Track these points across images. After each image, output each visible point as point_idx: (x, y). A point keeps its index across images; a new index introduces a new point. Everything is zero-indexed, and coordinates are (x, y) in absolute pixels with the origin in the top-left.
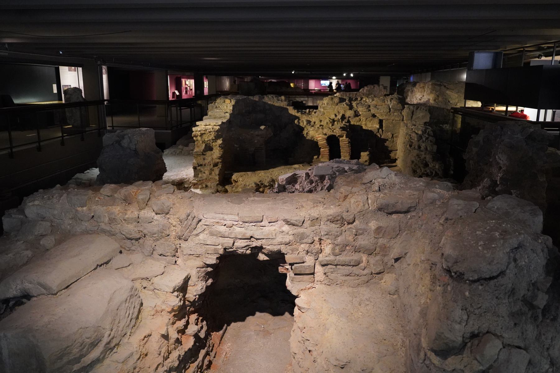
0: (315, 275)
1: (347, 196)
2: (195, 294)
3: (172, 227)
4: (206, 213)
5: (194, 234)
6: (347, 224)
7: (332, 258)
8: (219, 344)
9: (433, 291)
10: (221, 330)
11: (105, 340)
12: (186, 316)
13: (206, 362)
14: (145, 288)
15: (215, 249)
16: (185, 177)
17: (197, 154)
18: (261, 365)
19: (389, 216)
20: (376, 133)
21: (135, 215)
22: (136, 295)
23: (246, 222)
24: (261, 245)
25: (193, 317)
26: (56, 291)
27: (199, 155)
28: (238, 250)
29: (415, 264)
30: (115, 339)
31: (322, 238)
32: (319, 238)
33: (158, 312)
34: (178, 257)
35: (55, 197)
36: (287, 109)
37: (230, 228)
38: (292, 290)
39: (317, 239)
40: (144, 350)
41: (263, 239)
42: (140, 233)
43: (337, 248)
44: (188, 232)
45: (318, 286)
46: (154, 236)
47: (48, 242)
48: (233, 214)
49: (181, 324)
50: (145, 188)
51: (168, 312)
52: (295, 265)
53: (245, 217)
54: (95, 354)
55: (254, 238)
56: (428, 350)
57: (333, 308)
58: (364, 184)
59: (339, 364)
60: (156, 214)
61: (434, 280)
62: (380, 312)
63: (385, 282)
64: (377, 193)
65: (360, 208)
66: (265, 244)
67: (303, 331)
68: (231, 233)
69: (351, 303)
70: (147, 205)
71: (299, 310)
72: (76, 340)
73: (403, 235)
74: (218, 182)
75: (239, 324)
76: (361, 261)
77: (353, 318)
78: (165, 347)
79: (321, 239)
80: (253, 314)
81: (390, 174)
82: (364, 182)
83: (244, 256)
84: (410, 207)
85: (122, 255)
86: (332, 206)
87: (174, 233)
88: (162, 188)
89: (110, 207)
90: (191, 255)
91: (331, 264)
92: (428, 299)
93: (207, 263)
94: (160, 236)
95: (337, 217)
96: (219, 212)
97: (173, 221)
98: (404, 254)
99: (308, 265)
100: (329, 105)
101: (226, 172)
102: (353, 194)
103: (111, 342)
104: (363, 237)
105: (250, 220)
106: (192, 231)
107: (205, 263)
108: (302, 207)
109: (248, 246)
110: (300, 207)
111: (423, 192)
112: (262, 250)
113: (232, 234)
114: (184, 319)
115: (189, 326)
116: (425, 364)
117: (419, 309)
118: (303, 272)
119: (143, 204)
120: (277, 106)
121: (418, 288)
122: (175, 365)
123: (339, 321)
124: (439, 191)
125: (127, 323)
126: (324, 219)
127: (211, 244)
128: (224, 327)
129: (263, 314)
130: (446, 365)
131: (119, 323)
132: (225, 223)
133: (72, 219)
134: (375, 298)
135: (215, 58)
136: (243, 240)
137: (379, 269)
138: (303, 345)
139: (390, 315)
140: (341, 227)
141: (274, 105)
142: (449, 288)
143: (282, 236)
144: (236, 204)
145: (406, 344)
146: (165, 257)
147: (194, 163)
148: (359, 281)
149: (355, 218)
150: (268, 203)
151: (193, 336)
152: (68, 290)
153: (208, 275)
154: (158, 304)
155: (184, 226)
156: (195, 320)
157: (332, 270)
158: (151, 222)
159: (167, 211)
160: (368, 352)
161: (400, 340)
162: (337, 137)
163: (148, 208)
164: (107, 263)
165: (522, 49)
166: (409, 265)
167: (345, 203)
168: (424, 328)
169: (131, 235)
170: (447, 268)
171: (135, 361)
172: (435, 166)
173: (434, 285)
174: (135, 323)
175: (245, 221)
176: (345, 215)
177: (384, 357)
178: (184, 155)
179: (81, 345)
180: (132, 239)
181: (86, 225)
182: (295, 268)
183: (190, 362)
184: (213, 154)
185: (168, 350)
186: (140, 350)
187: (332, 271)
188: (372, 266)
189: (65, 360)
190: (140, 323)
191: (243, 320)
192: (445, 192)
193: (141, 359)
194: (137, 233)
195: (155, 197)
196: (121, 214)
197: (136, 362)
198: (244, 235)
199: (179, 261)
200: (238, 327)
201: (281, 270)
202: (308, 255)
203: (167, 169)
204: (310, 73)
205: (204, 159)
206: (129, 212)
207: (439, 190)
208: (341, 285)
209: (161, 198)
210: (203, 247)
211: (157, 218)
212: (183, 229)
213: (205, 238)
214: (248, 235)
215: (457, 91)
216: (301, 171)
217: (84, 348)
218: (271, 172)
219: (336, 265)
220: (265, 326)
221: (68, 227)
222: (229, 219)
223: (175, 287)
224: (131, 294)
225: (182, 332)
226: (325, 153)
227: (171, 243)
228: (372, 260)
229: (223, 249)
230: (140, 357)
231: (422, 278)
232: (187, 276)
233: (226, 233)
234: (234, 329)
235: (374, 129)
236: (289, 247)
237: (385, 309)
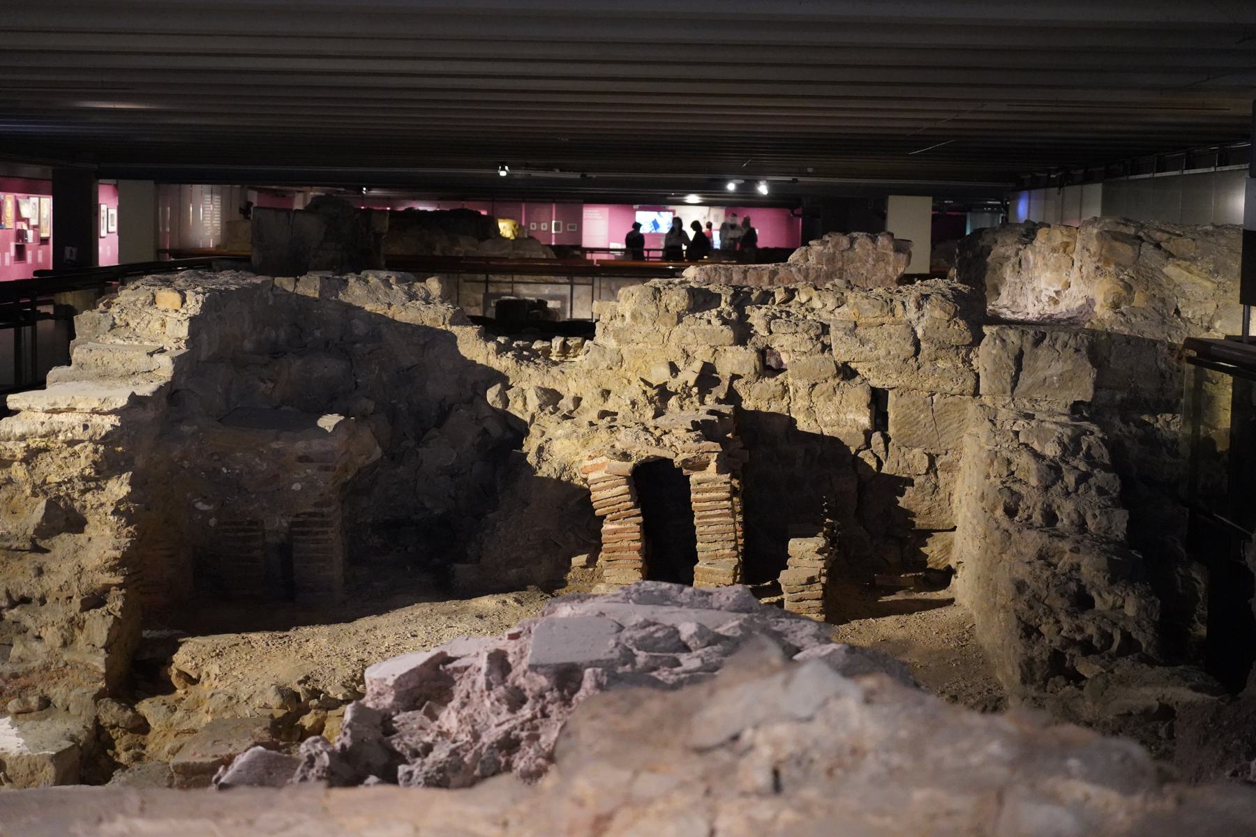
17: (9, 549)
20: (858, 451)
27: (17, 550)
36: (453, 338)
74: (102, 684)
101: (145, 633)
120: (407, 324)
141: (393, 321)
162: (680, 470)
172: (1122, 607)
204: (578, 176)
205: (40, 572)
207: (1078, 789)
218: (362, 632)
226: (625, 544)
235: (848, 433)
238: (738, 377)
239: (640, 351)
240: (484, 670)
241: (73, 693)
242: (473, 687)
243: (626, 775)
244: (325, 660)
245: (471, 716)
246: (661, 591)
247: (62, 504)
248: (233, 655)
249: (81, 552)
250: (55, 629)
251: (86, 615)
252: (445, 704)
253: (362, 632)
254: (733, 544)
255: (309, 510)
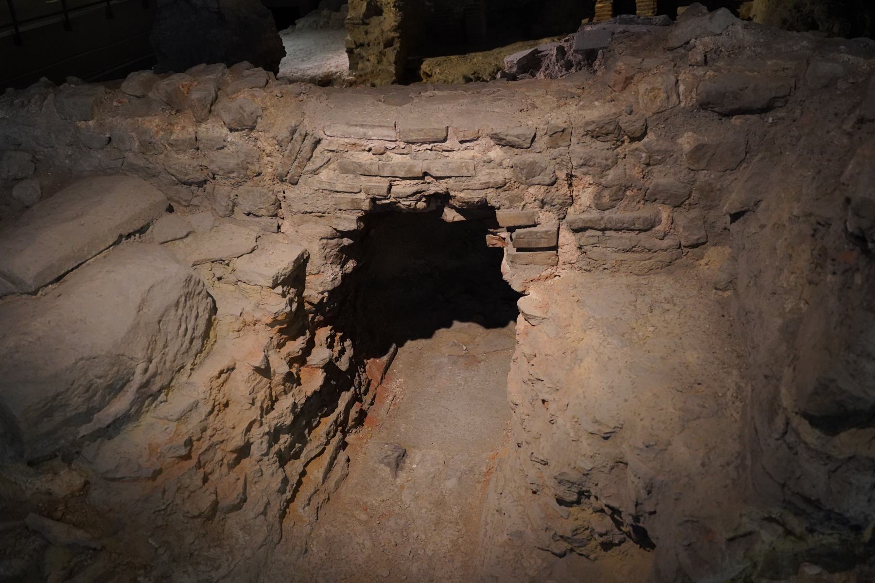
0: (559, 250)
1: (632, 78)
2: (321, 289)
3: (265, 158)
4: (329, 126)
5: (308, 171)
6: (628, 140)
7: (595, 214)
8: (382, 379)
9: (817, 284)
10: (384, 355)
11: (138, 379)
12: (307, 331)
13: (353, 414)
14: (219, 279)
15: (353, 201)
16: (333, 70)
17: (354, 24)
18: (459, 420)
19: (724, 119)
21: (190, 134)
22: (199, 294)
23: (413, 143)
24: (445, 190)
25: (323, 333)
26: (33, 287)
27: (357, 24)
28: (399, 202)
29: (776, 226)
30: (158, 378)
31: (573, 173)
32: (567, 174)
33: (246, 325)
34: (283, 219)
35: (33, 100)
37: (381, 157)
38: (512, 281)
39: (562, 175)
40: (220, 396)
41: (450, 177)
42: (205, 171)
43: (606, 193)
44: (297, 166)
45: (564, 273)
46: (232, 175)
47: (26, 191)
48: (383, 126)
49: (296, 346)
50: (208, 77)
51: (267, 324)
52: (517, 230)
53: (410, 131)
54: (120, 405)
55: (432, 176)
56: (794, 414)
57: (593, 317)
58: (671, 49)
59: (599, 430)
60: (231, 130)
61: (821, 259)
62: (694, 326)
63: (707, 264)
64: (700, 69)
65: (659, 104)
66: (454, 188)
67: (532, 362)
68: (384, 166)
69: (632, 308)
70: (210, 111)
71: (526, 320)
72: (74, 381)
73: (754, 161)
74: (394, 78)
75: (422, 342)
76: (657, 219)
77: (635, 337)
78: (264, 389)
79: (572, 176)
80: (448, 325)
81: (732, 24)
82: (671, 45)
83: (413, 213)
84: (774, 98)
85: (172, 216)
86: (596, 103)
87: (270, 170)
88: (243, 76)
89: (140, 119)
90: (306, 212)
91: (592, 228)
92: (803, 302)
93: (341, 228)
94: (242, 175)
95: (607, 126)
96: (355, 123)
97: (265, 144)
98: (752, 204)
99: (544, 229)
101: (409, 58)
102: (645, 74)
103: (151, 384)
104: (664, 169)
105: (422, 137)
106: (304, 163)
107: (335, 229)
108: (534, 107)
109: (420, 192)
110: (530, 107)
111: (807, 61)
112: (450, 201)
113: (386, 169)
114: (302, 338)
115: (314, 351)
116: (785, 441)
117: (779, 321)
118: (533, 246)
119: (203, 110)
121: (781, 278)
122: (285, 423)
123: (605, 343)
124: (846, 59)
125: (184, 346)
126: (577, 131)
127: (344, 190)
128: (392, 350)
129: (466, 325)
130: (835, 447)
131: (165, 346)
132: (371, 146)
133: (72, 145)
134: (683, 298)
136: (409, 182)
137: (696, 237)
138: (532, 390)
139: (715, 331)
140: (616, 148)
142: (858, 279)
143: (488, 171)
144: (393, 105)
145: (744, 393)
146: (257, 219)
147: (347, 41)
148: (652, 261)
149: (646, 128)
150: (461, 101)
151: (322, 368)
152: (60, 285)
153: (344, 254)
154: (247, 309)
155: (286, 153)
156: (327, 338)
157: (595, 240)
158: (222, 148)
159: (250, 124)
160: (662, 409)
161: (733, 385)
163: (214, 120)
164: (142, 231)
166: (763, 227)
167: (625, 94)
168: (789, 366)
169: (187, 174)
170: (857, 232)
171: (203, 417)
172: (832, 28)
173: (819, 269)
174: (203, 346)
175: (409, 139)
176: (624, 121)
177: (694, 419)
179: (87, 391)
180: (190, 184)
181: (99, 156)
182: (518, 237)
183: (320, 414)
184: (382, 22)
185: (271, 395)
186: (212, 397)
187: (595, 242)
188: (681, 230)
189: (58, 417)
190: (212, 345)
191: (428, 335)
192: (862, 59)
193: (216, 412)
194: (198, 171)
195: (228, 95)
196: (162, 133)
197: (206, 419)
198: (409, 170)
199: (286, 226)
200: (419, 348)
201: (491, 240)
202: (545, 209)
203: (286, 50)
205: (366, 33)
206: (177, 129)
207: (846, 57)
208: (615, 270)
209: (238, 96)
210: (329, 196)
211: (233, 140)
212: (286, 161)
213: (331, 179)
214: (418, 170)
216: (548, 46)
217: (94, 395)
218: (495, 54)
219: (603, 230)
220: (469, 347)
221: (67, 161)
222: (378, 137)
223: (277, 277)
224: (186, 291)
225: (301, 359)
226: (605, 13)
227: (265, 191)
228: (682, 218)
229: (369, 200)
230: (213, 410)
231: (791, 256)
232: (303, 254)
233: (373, 166)
234: (411, 352)
236: (503, 194)
237: (705, 319)
240: (555, 55)
241: (384, 82)
242: (550, 62)
243: (640, 60)
244: (482, 65)
245: (550, 73)
246: (631, 18)
247: (373, 4)
248: (445, 65)
249: (382, 24)
250: (374, 56)
251: (386, 50)
252: (538, 70)
253: (495, 54)
254: (653, 10)
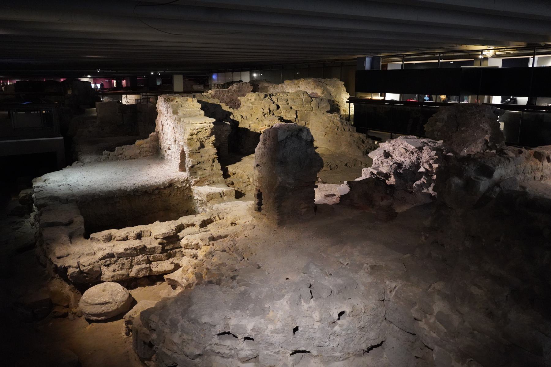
36: (220, 106)
100: (257, 101)
135: (99, 56)
165: (438, 55)
178: (112, 160)
204: (115, 71)
215: (333, 86)
235: (292, 119)
238: (274, 110)
239: (256, 106)
255: (223, 141)
